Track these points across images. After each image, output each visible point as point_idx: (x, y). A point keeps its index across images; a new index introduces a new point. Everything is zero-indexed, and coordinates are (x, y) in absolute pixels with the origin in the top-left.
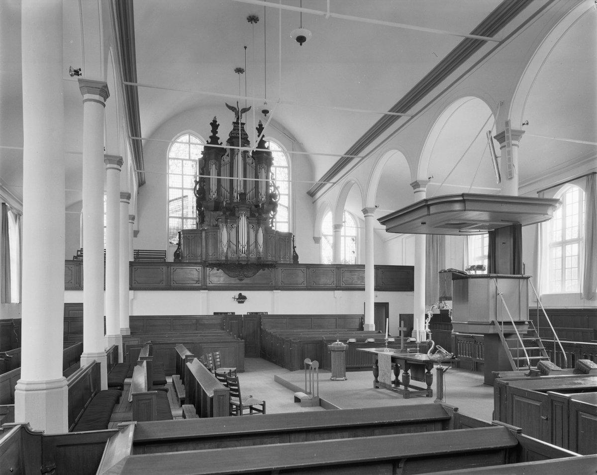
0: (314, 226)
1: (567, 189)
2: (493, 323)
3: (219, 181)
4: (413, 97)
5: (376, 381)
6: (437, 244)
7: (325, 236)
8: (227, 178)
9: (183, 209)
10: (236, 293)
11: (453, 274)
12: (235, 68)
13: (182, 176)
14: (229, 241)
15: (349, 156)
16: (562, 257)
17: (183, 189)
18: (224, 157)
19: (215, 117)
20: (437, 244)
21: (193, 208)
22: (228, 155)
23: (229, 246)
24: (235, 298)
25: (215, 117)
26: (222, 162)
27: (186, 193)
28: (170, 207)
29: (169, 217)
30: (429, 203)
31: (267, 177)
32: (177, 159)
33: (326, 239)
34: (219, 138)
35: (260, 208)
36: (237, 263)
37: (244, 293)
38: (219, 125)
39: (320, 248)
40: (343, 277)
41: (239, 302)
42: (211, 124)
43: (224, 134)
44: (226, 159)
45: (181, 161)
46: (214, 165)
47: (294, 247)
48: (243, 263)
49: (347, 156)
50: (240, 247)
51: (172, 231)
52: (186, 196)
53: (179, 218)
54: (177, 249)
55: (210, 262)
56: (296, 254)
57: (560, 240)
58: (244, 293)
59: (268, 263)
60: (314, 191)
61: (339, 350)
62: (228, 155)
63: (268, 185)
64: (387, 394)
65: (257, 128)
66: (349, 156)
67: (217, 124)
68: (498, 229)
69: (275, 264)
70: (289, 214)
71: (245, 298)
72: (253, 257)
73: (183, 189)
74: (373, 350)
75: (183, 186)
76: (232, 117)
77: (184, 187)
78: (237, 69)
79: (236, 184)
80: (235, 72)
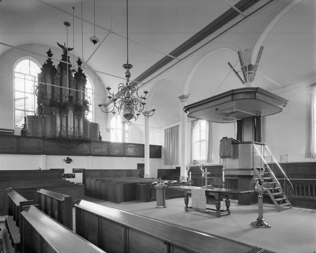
0: (107, 125)
1: (200, 121)
2: (253, 169)
3: (53, 88)
4: (186, 47)
5: (187, 207)
6: (174, 135)
7: (112, 129)
8: (58, 86)
9: (25, 105)
10: (65, 157)
11: (232, 141)
12: (64, 22)
13: (25, 80)
14: (61, 125)
15: (136, 82)
16: (200, 146)
17: (25, 92)
18: (57, 74)
19: (50, 49)
20: (174, 135)
21: (32, 105)
22: (59, 74)
23: (61, 128)
24: (64, 160)
25: (50, 49)
26: (55, 77)
27: (27, 95)
28: (16, 103)
29: (15, 109)
30: (235, 92)
31: (84, 90)
32: (21, 73)
33: (113, 130)
34: (52, 62)
35: (80, 108)
36: (66, 138)
37: (70, 157)
38: (52, 54)
39: (110, 135)
40: (122, 150)
41: (67, 163)
42: (47, 53)
43: (56, 61)
44: (58, 76)
45: (24, 75)
46: (49, 78)
47: (99, 132)
48: (71, 139)
49: (135, 82)
50: (69, 129)
51: (17, 118)
52: (27, 98)
53: (22, 110)
54: (24, 128)
55: (48, 137)
56: (101, 136)
57: (199, 140)
58: (70, 157)
59: (86, 139)
60: (108, 104)
61: (160, 188)
62: (59, 74)
63: (84, 95)
64: (206, 217)
65: (77, 61)
66: (136, 82)
67: (51, 53)
68: (243, 119)
69: (85, 141)
70: (93, 115)
71: (71, 160)
72: (74, 137)
73: (25, 92)
74: (186, 187)
75: (25, 90)
76: (61, 52)
77: (26, 91)
78: (66, 22)
79: (64, 92)
80: (64, 24)
